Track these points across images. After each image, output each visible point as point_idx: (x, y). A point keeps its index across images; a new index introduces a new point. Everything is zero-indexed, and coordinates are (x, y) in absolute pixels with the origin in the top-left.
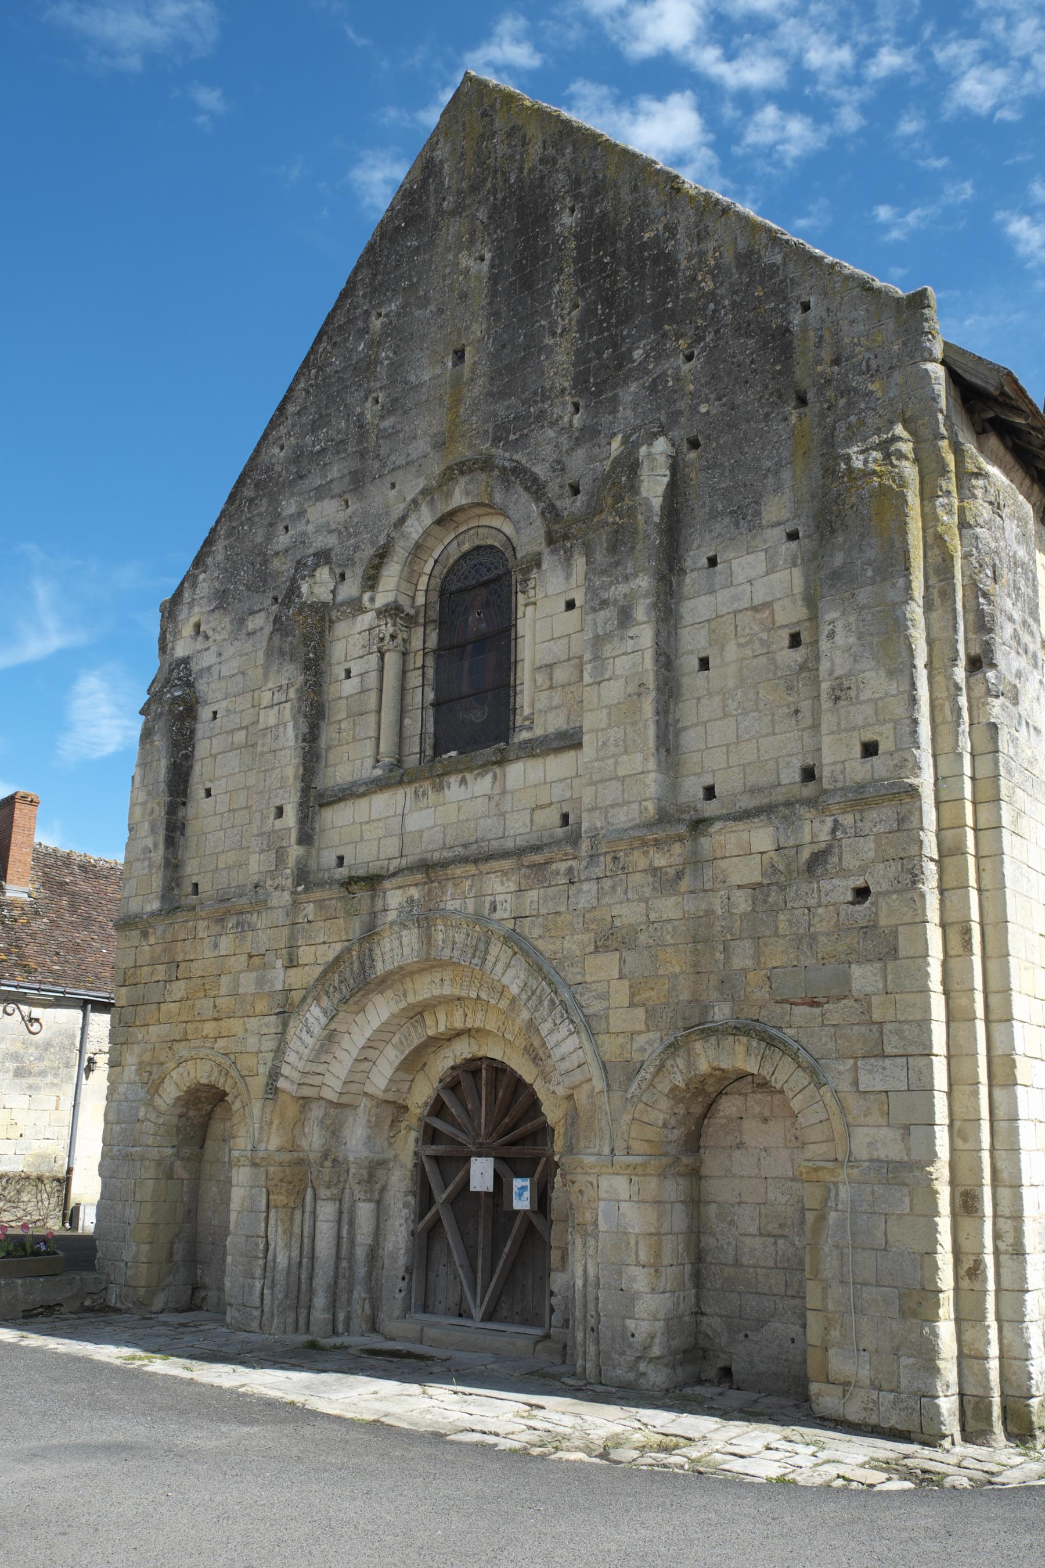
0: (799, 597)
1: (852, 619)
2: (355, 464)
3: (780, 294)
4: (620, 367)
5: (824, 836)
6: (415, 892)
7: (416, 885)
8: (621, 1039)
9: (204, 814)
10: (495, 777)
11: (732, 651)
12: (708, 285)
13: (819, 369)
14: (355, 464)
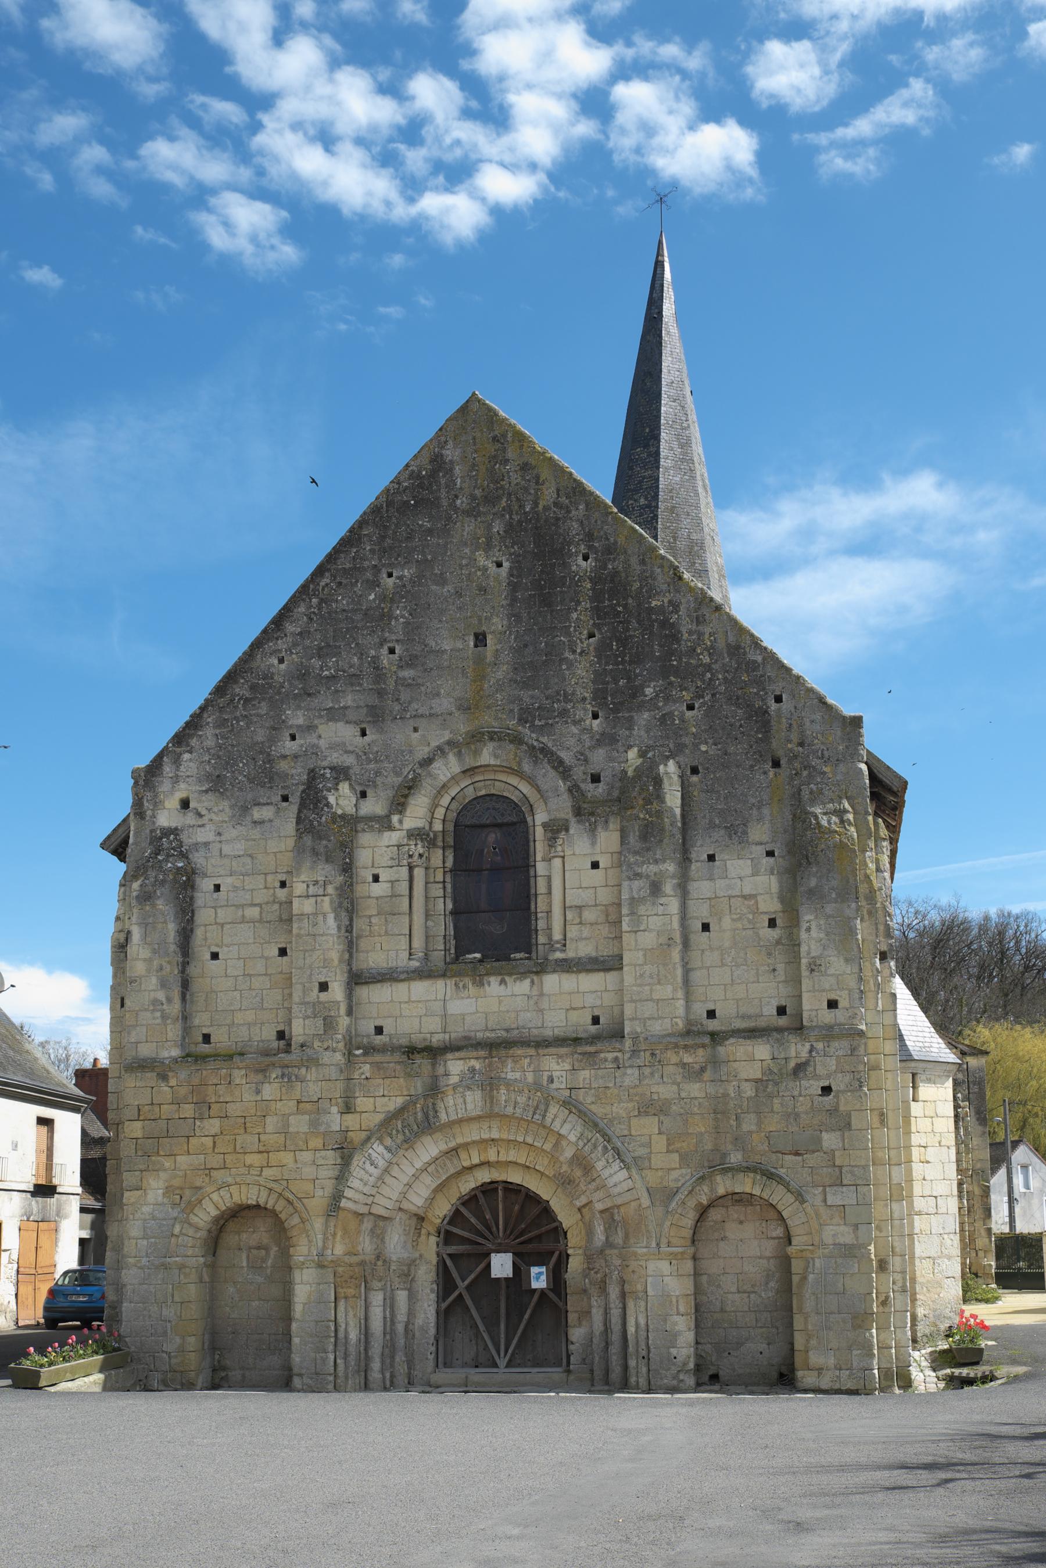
0: (775, 896)
1: (822, 922)
2: (373, 700)
3: (759, 682)
4: (634, 696)
5: (804, 1054)
6: (477, 1065)
7: (477, 1058)
8: (660, 1173)
9: (209, 974)
10: (532, 982)
11: (727, 922)
12: (706, 660)
13: (790, 746)
14: (373, 700)
